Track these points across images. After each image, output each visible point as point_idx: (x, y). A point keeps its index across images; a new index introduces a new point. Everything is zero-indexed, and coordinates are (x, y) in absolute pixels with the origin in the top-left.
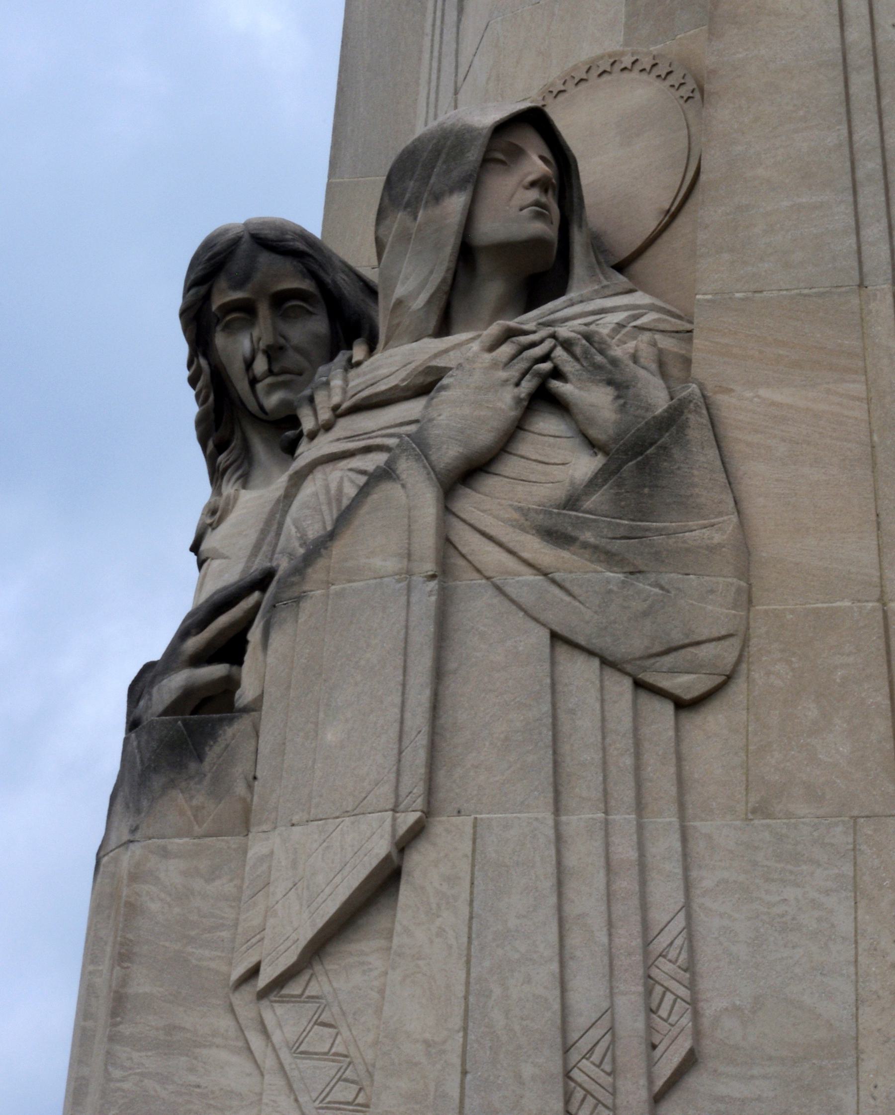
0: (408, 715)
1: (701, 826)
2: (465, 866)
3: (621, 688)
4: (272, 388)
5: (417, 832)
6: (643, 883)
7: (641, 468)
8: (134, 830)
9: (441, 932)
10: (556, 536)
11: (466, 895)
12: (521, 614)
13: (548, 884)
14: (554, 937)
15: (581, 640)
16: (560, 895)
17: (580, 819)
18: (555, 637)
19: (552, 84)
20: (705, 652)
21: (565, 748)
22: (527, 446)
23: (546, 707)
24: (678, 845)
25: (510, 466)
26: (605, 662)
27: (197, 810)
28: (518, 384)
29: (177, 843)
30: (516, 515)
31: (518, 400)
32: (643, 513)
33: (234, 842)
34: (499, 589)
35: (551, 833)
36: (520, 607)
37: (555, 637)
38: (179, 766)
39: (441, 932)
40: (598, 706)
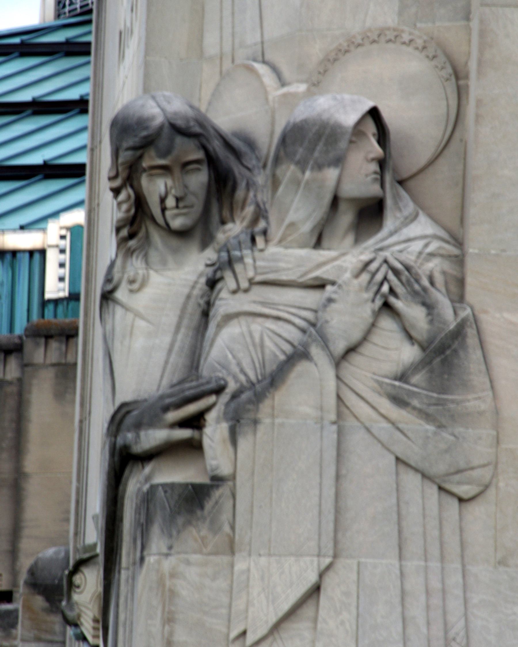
0: (323, 502)
1: (472, 569)
2: (353, 588)
3: (433, 491)
4: (176, 216)
5: (329, 567)
6: (444, 600)
7: (444, 362)
8: (170, 548)
9: (342, 623)
10: (398, 401)
11: (354, 604)
12: (380, 445)
13: (397, 600)
14: (400, 628)
15: (413, 464)
16: (403, 605)
17: (412, 565)
18: (398, 459)
19: (354, 37)
20: (475, 474)
21: (404, 524)
22: (376, 338)
23: (394, 501)
24: (461, 580)
25: (367, 349)
26: (425, 476)
27: (203, 539)
28: (373, 301)
29: (195, 557)
30: (376, 385)
31: (373, 312)
32: (444, 390)
33: (226, 559)
34: (368, 430)
35: (398, 572)
36: (379, 441)
37: (398, 459)
38: (191, 512)
39: (342, 623)
40: (420, 501)
